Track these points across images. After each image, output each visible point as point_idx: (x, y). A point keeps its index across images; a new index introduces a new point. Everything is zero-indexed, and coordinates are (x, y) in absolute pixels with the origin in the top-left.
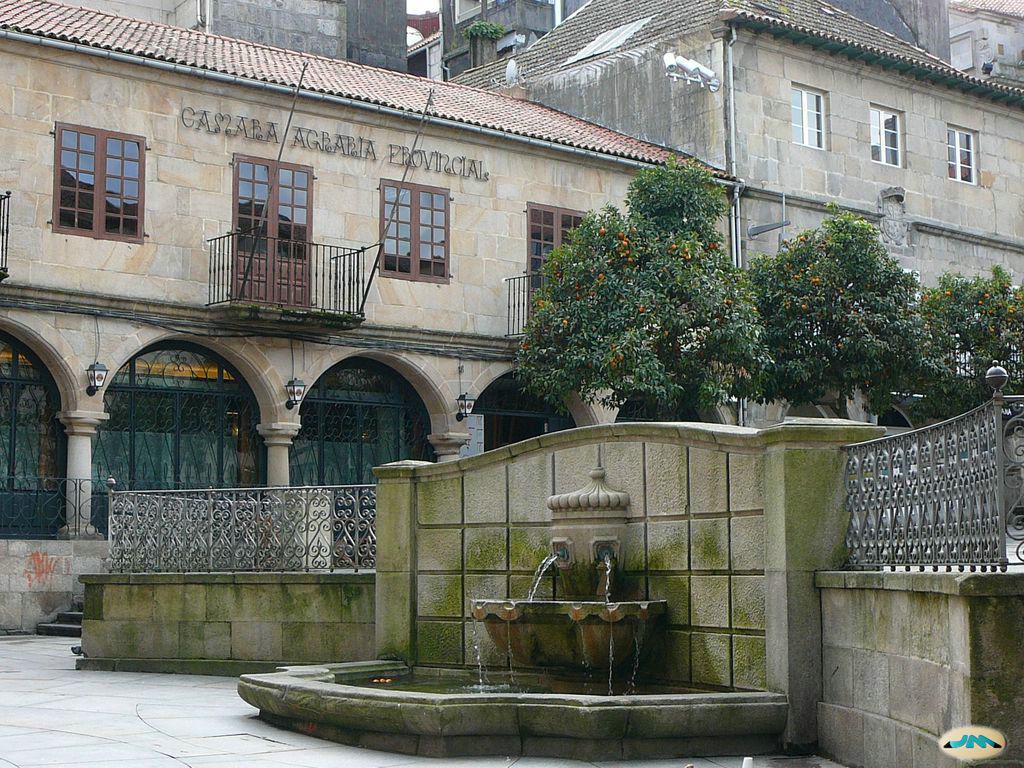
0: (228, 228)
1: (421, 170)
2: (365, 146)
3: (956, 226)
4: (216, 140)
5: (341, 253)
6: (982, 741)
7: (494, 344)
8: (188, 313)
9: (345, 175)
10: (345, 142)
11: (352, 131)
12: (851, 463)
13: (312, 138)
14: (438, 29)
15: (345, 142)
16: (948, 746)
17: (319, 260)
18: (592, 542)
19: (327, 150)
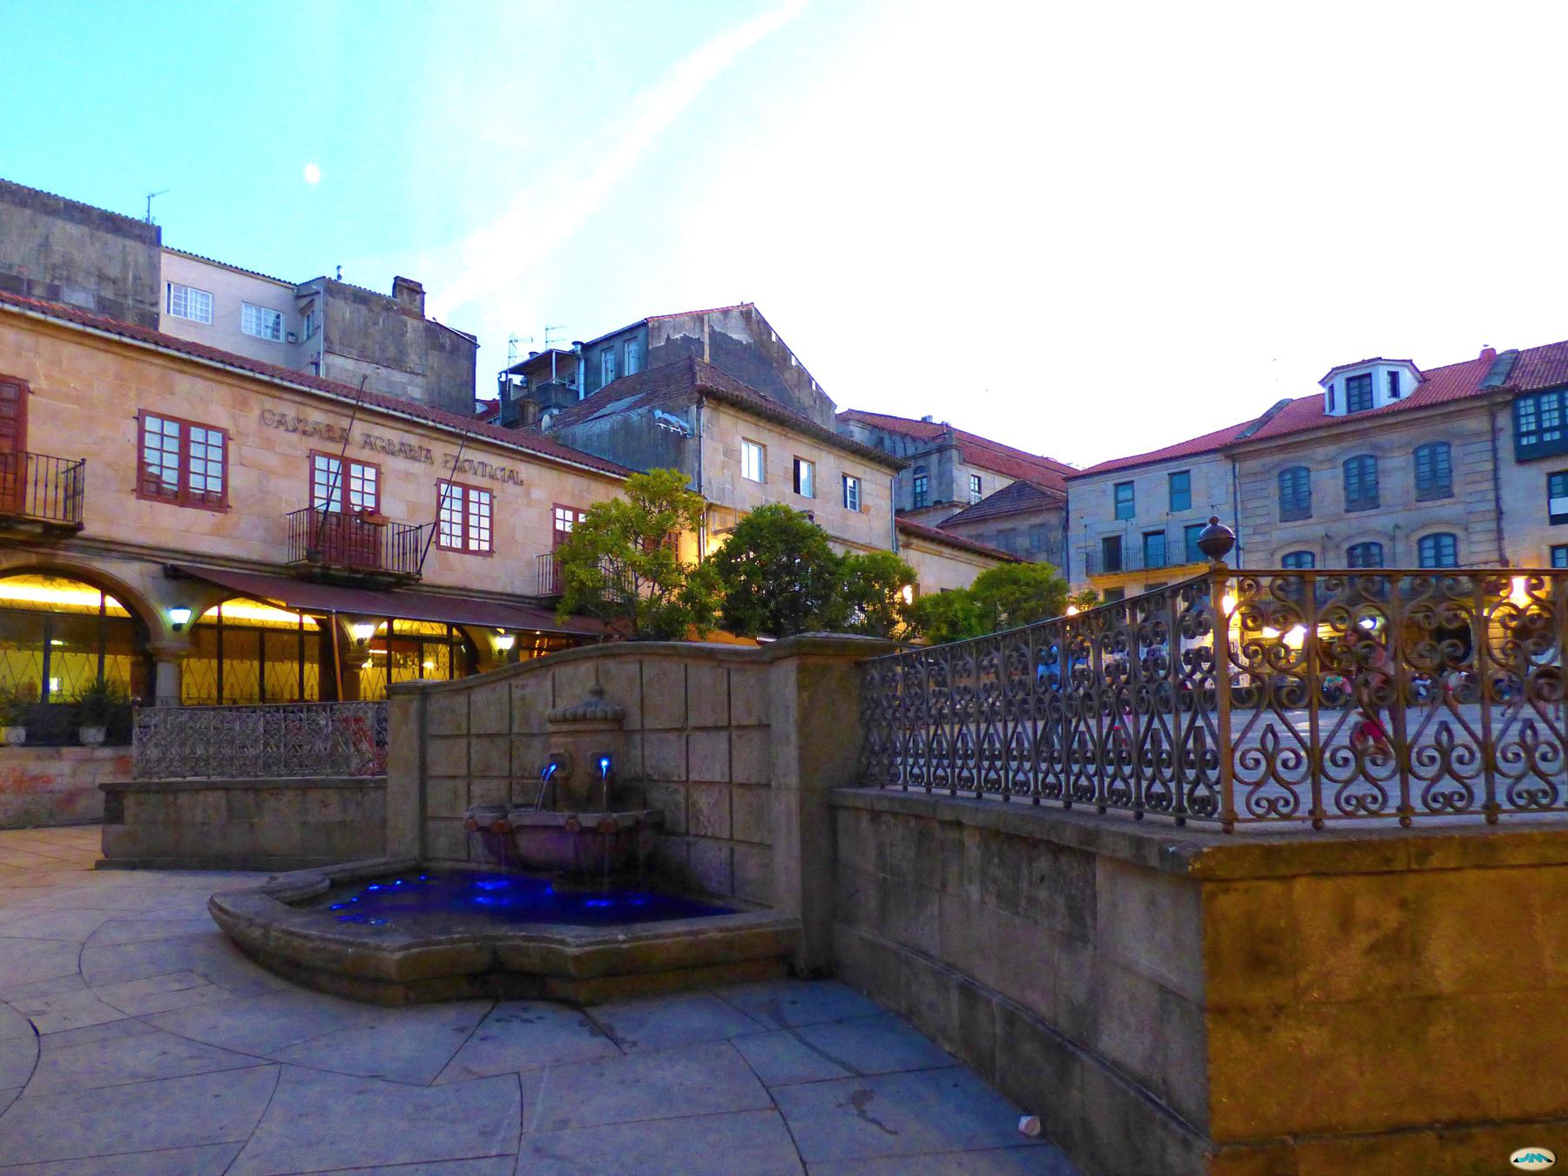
1: (471, 473)
3: (846, 537)
4: (294, 437)
5: (402, 530)
6: (1540, 1158)
7: (527, 601)
8: (269, 569)
11: (413, 440)
12: (868, 678)
13: (379, 443)
14: (498, 411)
16: (1516, 1161)
17: (387, 534)
18: (589, 754)
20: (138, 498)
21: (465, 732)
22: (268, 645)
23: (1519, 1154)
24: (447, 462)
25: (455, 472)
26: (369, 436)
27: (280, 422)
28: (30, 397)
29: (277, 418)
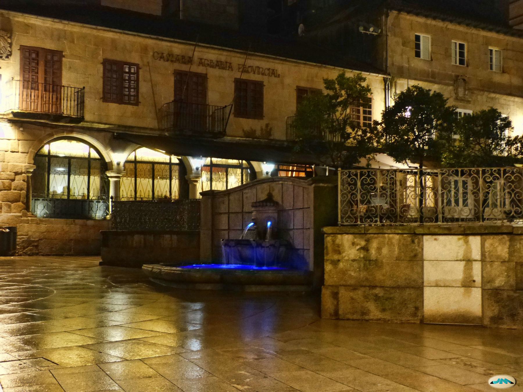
0: (172, 99)
2: (228, 64)
4: (167, 64)
5: (216, 108)
6: (506, 381)
9: (220, 77)
10: (220, 63)
15: (220, 63)
16: (492, 383)
19: (212, 67)
20: (103, 102)
21: (227, 212)
22: (138, 170)
23: (494, 379)
24: (239, 68)
25: (243, 73)
26: (201, 59)
27: (161, 58)
28: (63, 59)
29: (160, 55)
